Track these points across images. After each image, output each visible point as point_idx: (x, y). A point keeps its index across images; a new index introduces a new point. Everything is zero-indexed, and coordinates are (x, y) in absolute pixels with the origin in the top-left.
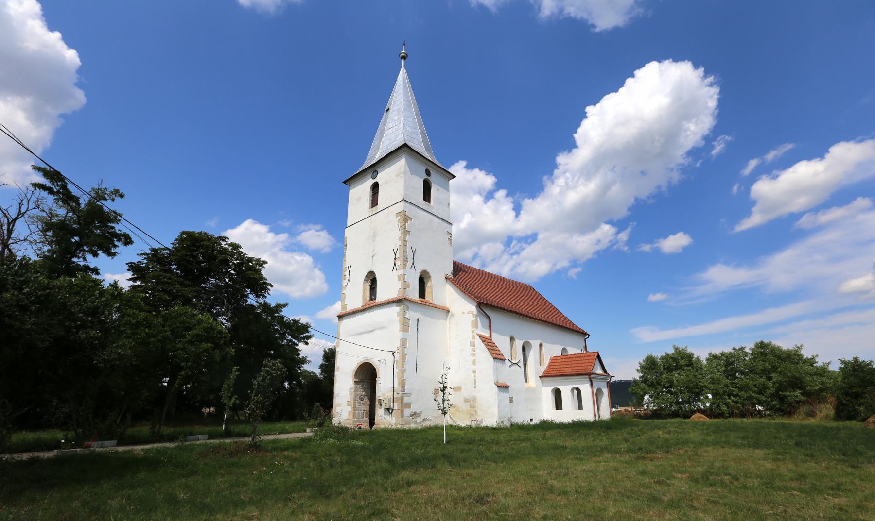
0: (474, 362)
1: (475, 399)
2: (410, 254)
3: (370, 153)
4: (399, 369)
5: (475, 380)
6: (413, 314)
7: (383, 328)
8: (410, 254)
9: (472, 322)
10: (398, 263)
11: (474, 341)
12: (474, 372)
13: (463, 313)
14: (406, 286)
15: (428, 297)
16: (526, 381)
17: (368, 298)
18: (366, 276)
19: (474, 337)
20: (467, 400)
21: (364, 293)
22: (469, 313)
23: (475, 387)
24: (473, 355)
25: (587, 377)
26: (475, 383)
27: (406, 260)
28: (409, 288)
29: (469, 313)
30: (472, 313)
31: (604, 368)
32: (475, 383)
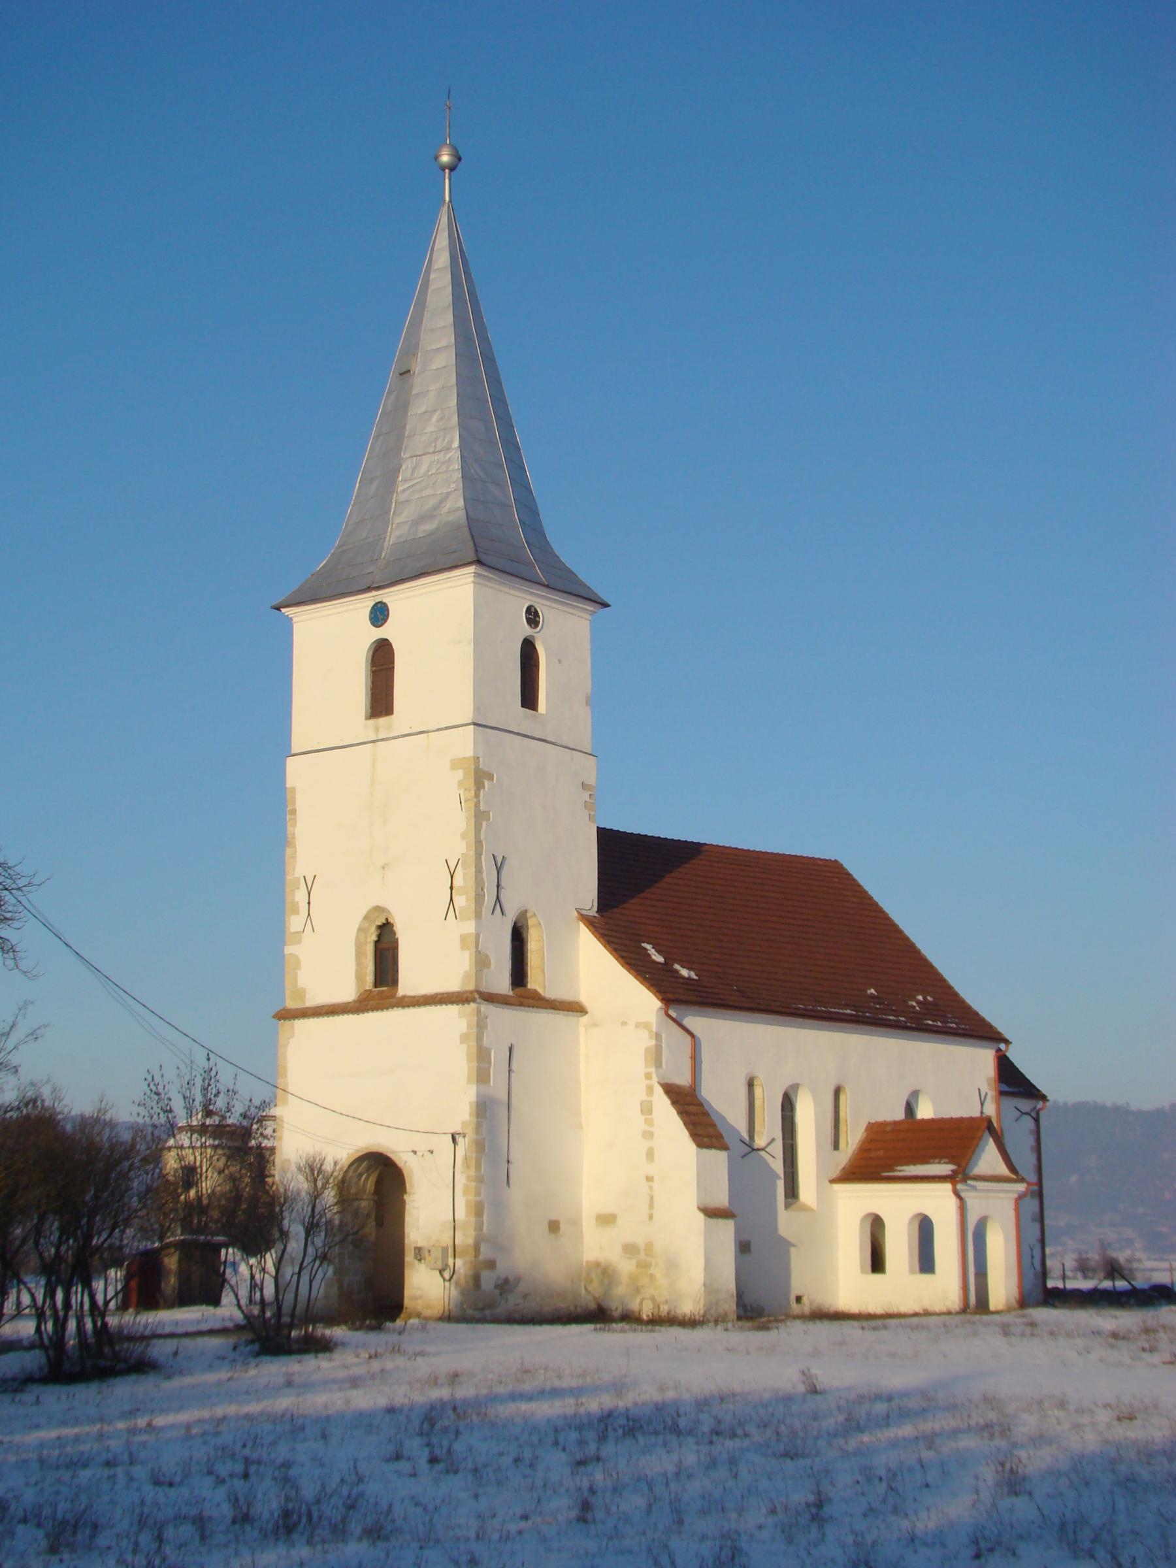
0: (650, 1155)
1: (649, 1246)
2: (498, 1057)
3: (454, 402)
4: (468, 1178)
5: (652, 1198)
6: (506, 1019)
7: (773, 1157)
8: (498, 1057)
9: (647, 1050)
10: (460, 901)
11: (651, 1102)
12: (649, 1179)
13: (624, 1023)
14: (481, 962)
15: (534, 982)
16: (529, 699)
17: (370, 978)
18: (365, 918)
19: (650, 1090)
20: (630, 1249)
21: (359, 963)
22: (638, 1025)
23: (651, 1217)
24: (648, 1135)
25: (948, 1187)
26: (651, 1206)
27: (479, 898)
28: (489, 966)
29: (638, 1025)
30: (646, 1026)
31: (1010, 1160)
32: (651, 1206)
